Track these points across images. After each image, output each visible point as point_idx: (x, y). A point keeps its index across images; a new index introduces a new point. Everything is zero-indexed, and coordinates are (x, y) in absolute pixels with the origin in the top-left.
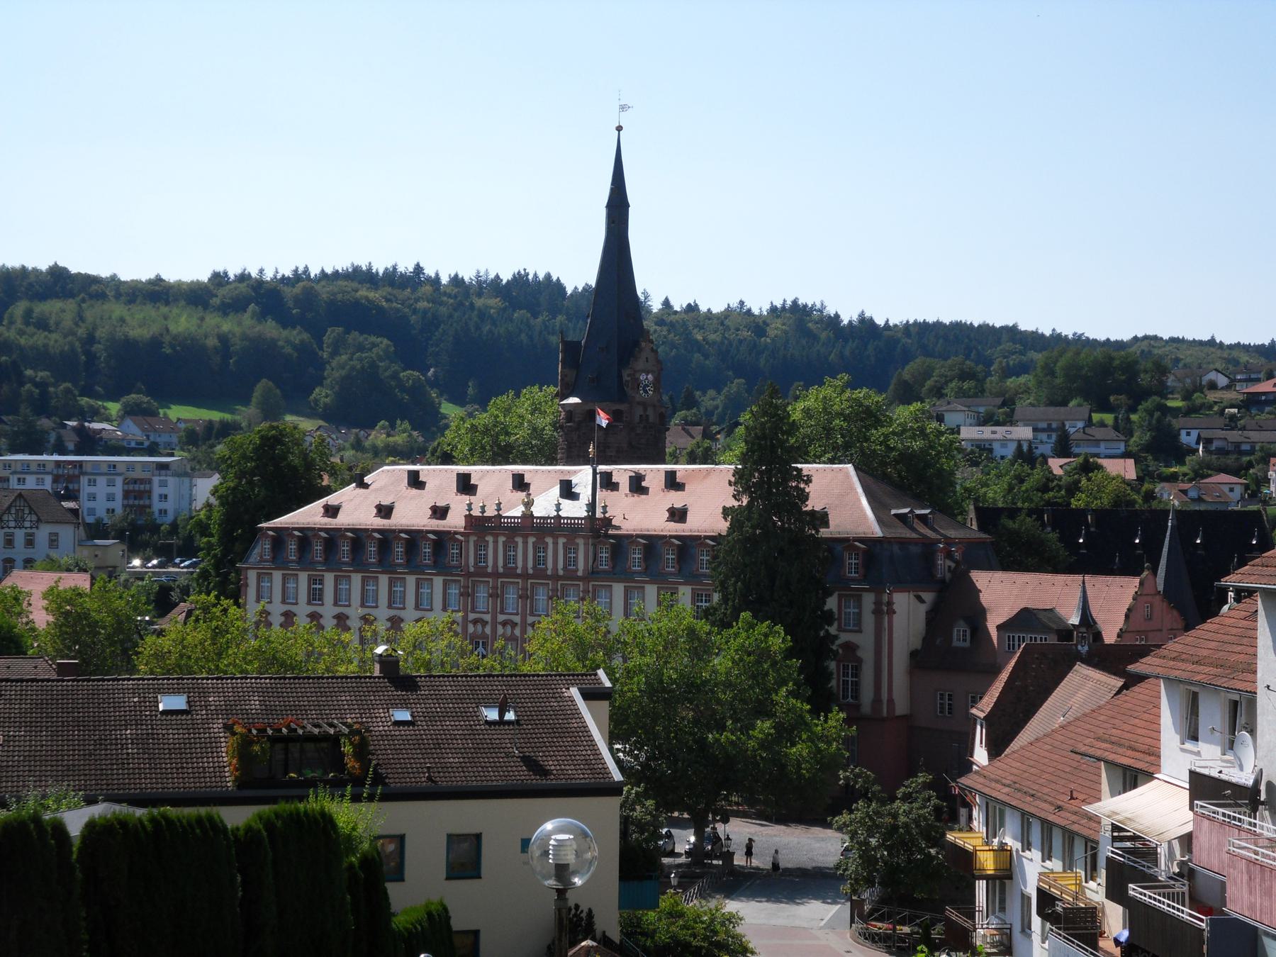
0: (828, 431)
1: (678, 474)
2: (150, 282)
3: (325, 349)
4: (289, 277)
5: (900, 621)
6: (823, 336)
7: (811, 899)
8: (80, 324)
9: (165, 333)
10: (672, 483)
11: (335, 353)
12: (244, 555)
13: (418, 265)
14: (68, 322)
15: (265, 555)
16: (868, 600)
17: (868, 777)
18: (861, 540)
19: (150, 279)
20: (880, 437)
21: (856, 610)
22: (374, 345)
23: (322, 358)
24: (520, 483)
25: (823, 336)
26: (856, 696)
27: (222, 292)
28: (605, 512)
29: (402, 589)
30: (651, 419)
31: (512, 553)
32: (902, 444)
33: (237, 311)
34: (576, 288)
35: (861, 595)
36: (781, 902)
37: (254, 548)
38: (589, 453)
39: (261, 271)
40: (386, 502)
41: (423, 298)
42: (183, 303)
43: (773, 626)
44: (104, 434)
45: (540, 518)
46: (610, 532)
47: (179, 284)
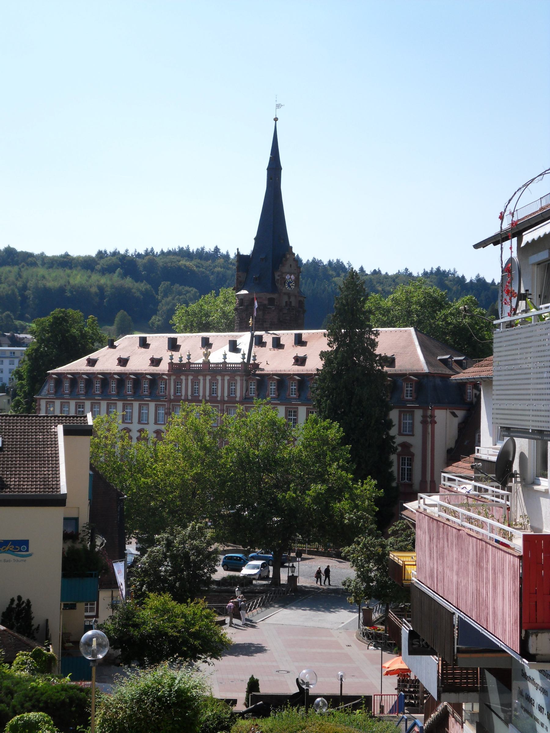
0: (409, 313)
1: (303, 336)
2: (62, 256)
3: (159, 294)
4: (142, 254)
5: (438, 428)
6: (454, 288)
7: (342, 609)
8: (19, 279)
9: (67, 284)
10: (299, 341)
11: (165, 295)
12: (38, 391)
13: (216, 247)
14: (12, 278)
15: (51, 390)
16: (418, 414)
17: (367, 518)
18: (415, 375)
19: (62, 255)
20: (442, 316)
21: (411, 421)
22: (188, 292)
23: (157, 299)
24: (206, 343)
25: (454, 288)
26: (410, 479)
27: (102, 261)
28: (255, 360)
29: (131, 411)
30: (293, 304)
31: (197, 387)
32: (456, 320)
33: (110, 273)
34: (308, 260)
35: (413, 411)
36: (319, 611)
37: (44, 386)
38: (249, 324)
39: (127, 251)
40: (124, 356)
41: (218, 266)
42: (79, 268)
43: (332, 423)
44: (25, 340)
45: (214, 364)
46: (257, 372)
47: (79, 257)
